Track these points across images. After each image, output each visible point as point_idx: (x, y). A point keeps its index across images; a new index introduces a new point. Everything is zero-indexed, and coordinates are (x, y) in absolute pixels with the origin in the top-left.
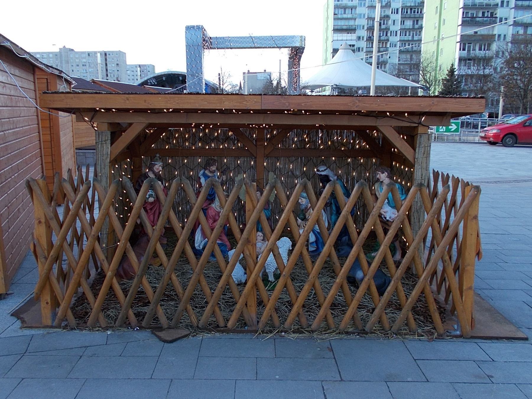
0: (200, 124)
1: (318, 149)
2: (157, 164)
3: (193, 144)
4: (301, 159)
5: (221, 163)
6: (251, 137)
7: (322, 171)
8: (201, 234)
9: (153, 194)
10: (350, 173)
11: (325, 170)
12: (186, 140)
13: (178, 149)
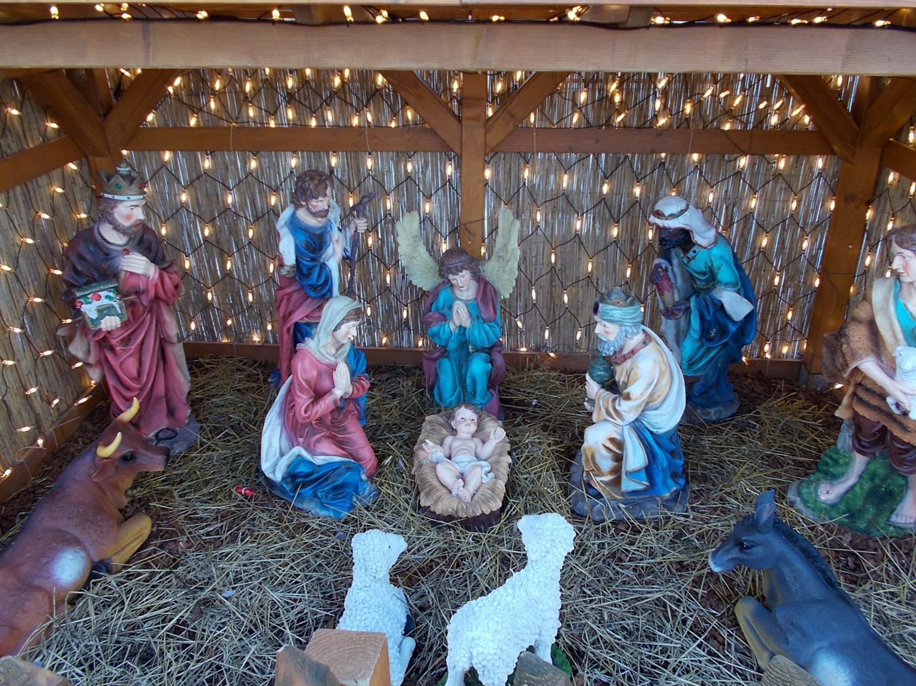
0: (162, 72)
1: (651, 127)
2: (122, 201)
3: (273, 112)
4: (597, 159)
5: (359, 171)
6: (445, 90)
7: (673, 216)
8: (278, 429)
9: (116, 305)
10: (741, 199)
11: (682, 212)
12: (247, 100)
13: (229, 128)
